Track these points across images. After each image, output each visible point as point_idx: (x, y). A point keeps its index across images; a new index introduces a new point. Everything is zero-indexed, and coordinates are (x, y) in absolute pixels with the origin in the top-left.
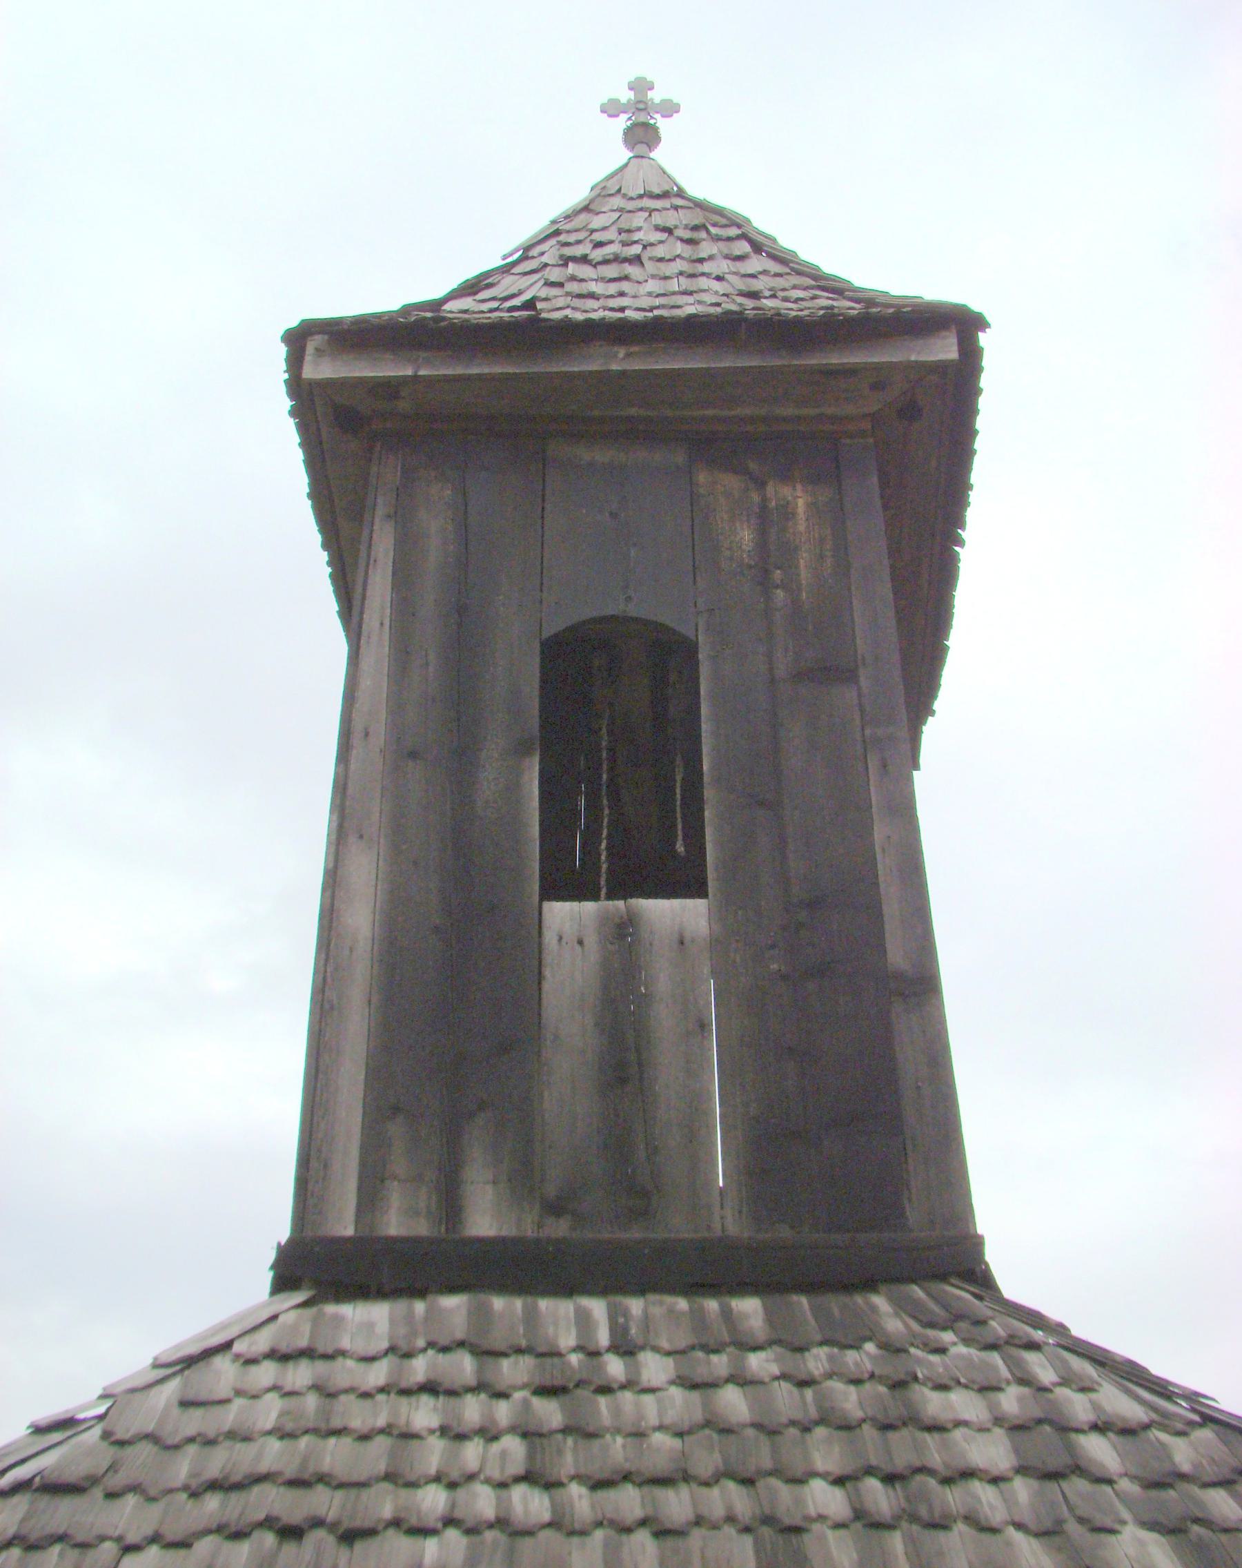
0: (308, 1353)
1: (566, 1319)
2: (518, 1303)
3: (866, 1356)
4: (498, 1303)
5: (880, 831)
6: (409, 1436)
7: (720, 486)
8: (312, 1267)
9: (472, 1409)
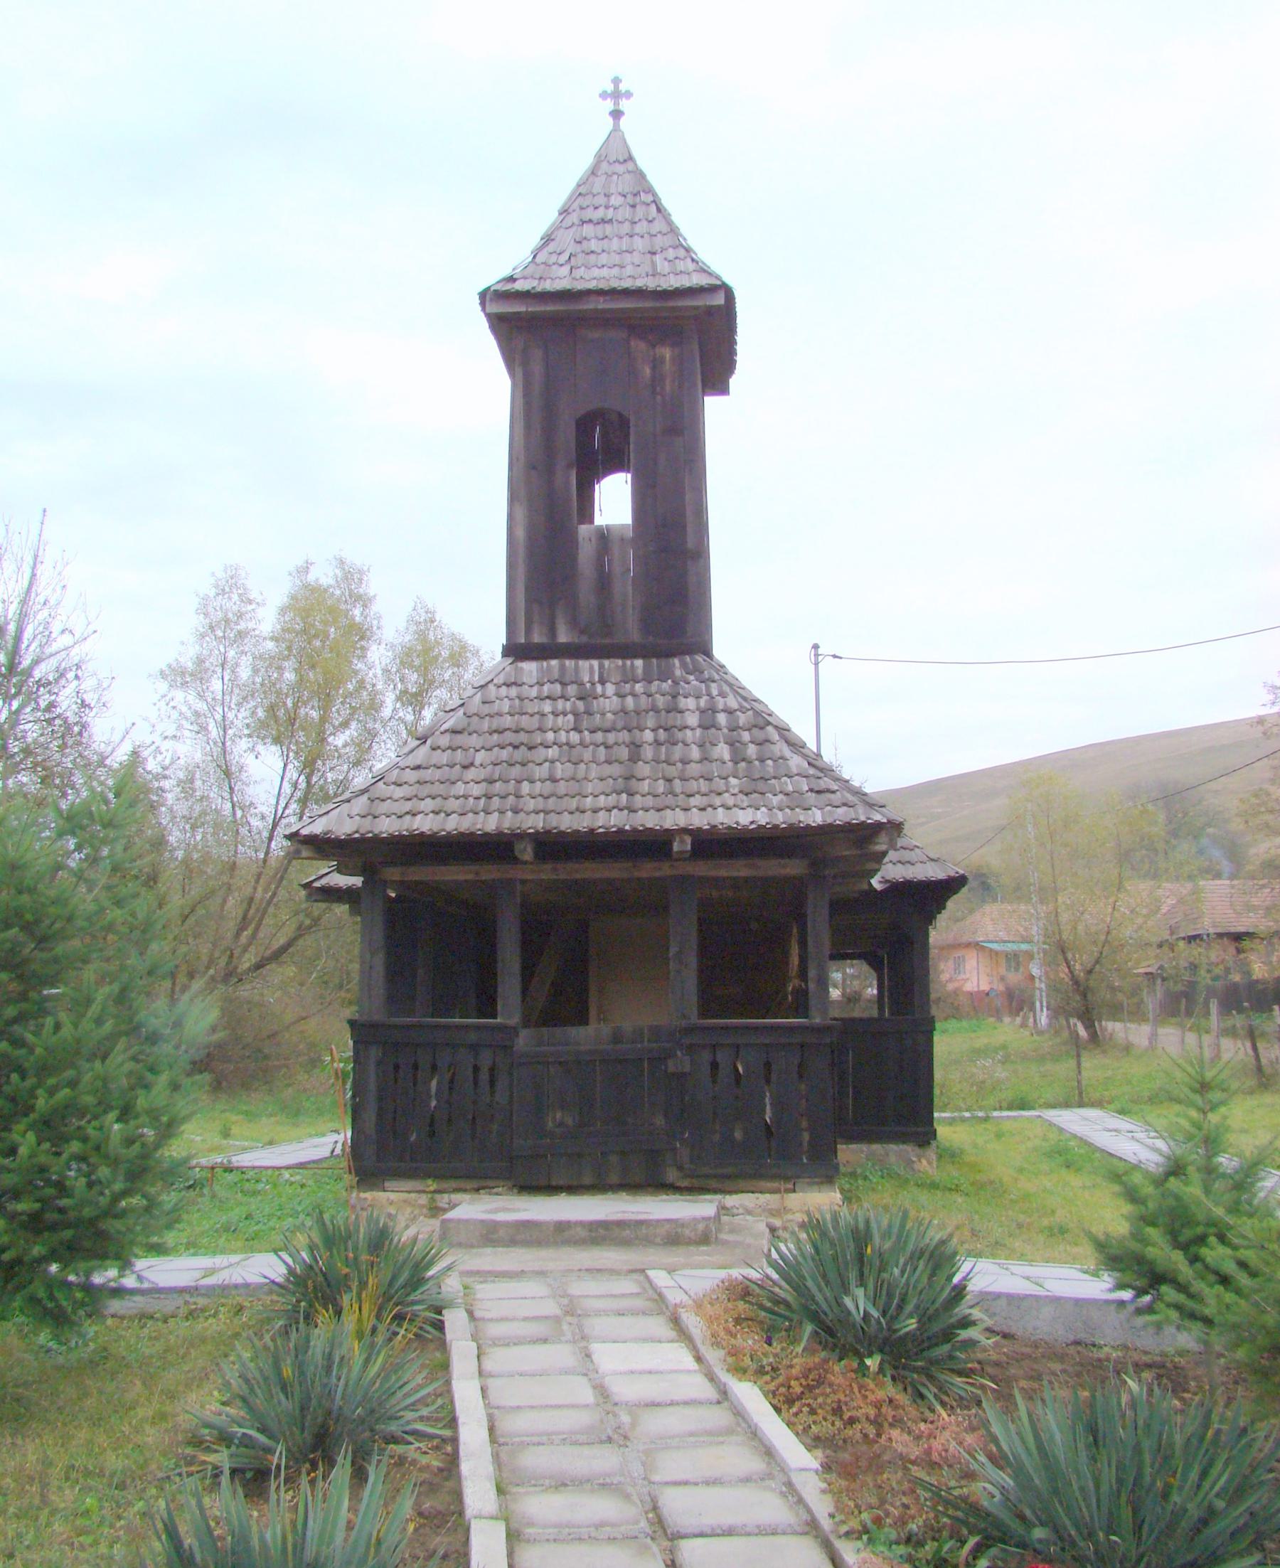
0: (515, 684)
1: (588, 668)
2: (573, 662)
3: (666, 686)
4: (567, 662)
5: (688, 497)
6: (543, 715)
7: (638, 346)
8: (514, 651)
9: (560, 704)
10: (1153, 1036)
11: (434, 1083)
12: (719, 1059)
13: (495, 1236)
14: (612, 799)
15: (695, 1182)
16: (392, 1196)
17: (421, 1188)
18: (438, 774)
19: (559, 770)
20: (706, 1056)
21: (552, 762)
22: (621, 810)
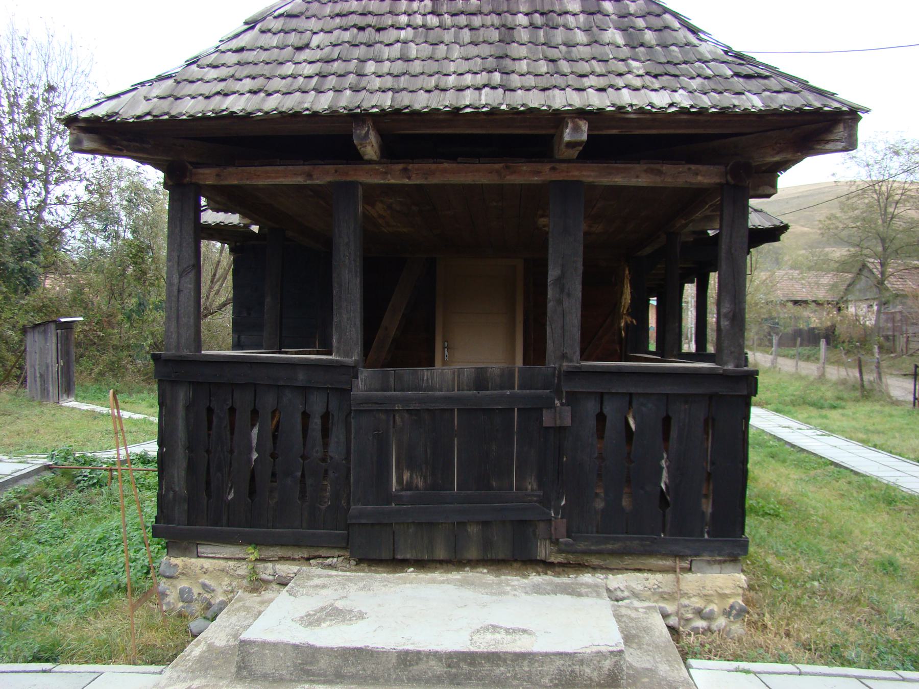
10: (774, 363)
11: (255, 431)
12: (606, 410)
13: (314, 668)
14: (481, 79)
15: (572, 558)
16: (207, 564)
17: (241, 556)
18: (264, 56)
19: (413, 51)
20: (591, 407)
21: (405, 42)
22: (494, 88)
